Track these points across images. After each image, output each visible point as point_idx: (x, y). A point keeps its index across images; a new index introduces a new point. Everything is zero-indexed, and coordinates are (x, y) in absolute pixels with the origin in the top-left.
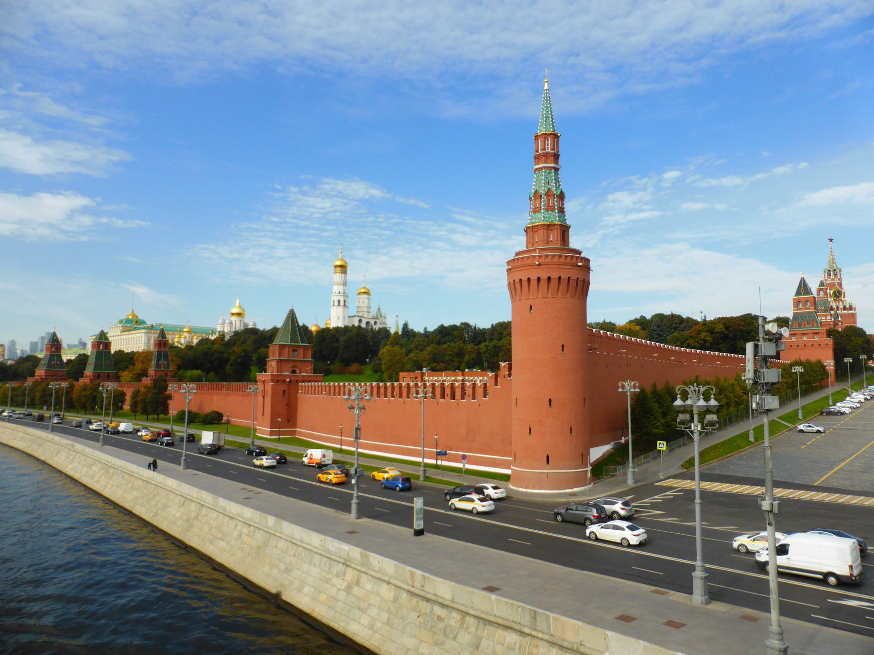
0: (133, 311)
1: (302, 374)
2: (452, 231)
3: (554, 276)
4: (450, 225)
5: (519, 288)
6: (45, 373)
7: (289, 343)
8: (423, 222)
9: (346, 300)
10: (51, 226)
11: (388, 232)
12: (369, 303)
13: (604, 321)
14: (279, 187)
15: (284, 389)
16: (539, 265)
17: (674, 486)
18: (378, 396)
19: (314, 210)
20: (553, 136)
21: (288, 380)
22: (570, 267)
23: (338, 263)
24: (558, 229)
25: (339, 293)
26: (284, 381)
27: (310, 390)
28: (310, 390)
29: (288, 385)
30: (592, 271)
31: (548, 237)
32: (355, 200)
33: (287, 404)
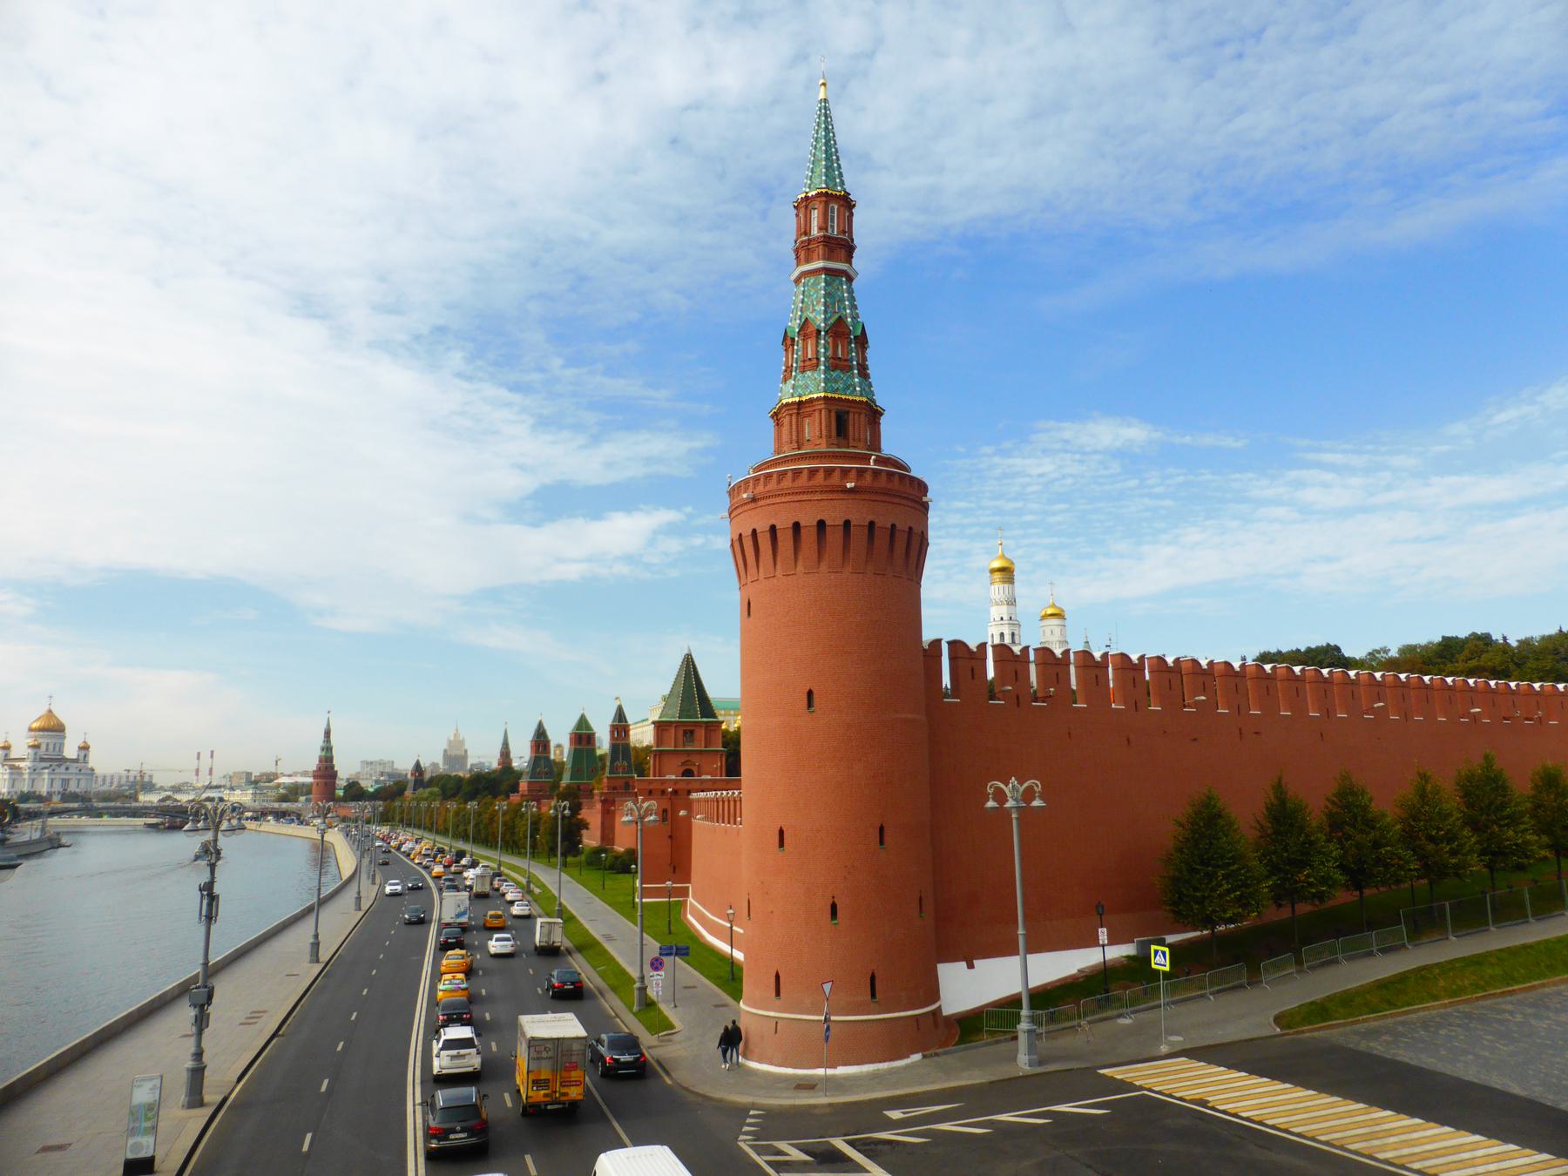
1: (703, 777)
2: (1300, 484)
3: (784, 522)
4: (1293, 474)
6: (528, 787)
7: (677, 719)
8: (1237, 476)
9: (1016, 632)
10: (629, 559)
11: (1168, 503)
12: (1063, 634)
13: (1561, 631)
14: (962, 450)
15: (665, 807)
16: (754, 500)
17: (1137, 1083)
19: (1027, 480)
20: (824, 199)
21: (670, 790)
22: (824, 496)
23: (997, 564)
25: (1002, 619)
26: (663, 792)
29: (670, 799)
31: (800, 431)
32: (1096, 452)
33: (671, 837)
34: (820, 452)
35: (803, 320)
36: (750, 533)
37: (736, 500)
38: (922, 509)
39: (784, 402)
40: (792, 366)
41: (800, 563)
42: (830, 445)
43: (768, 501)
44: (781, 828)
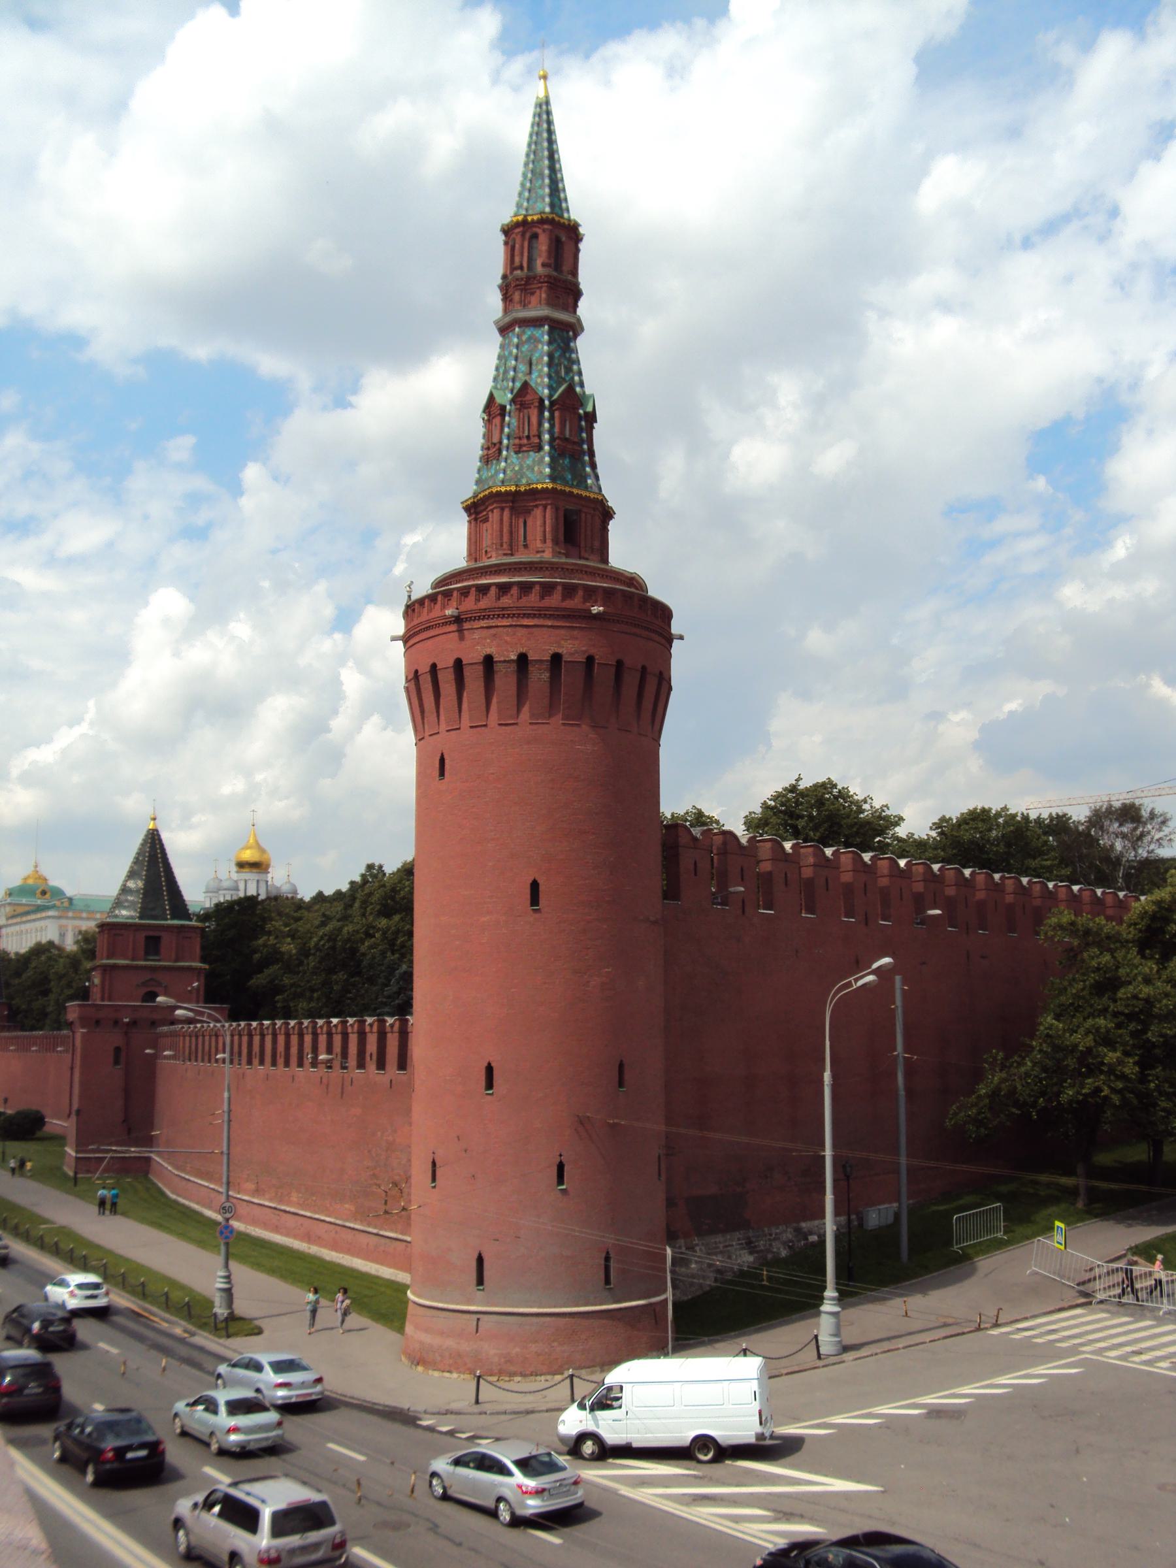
0: (36, 866)
5: (432, 698)
18: (361, 1065)
24: (545, 507)
26: (116, 1022)
27: (294, 1050)
28: (294, 1050)
30: (394, 639)
34: (521, 563)
35: (518, 385)
36: (428, 669)
37: (416, 622)
38: (663, 641)
39: (494, 490)
40: (501, 442)
41: (526, 709)
42: (556, 553)
43: (483, 623)
44: (489, 1064)
